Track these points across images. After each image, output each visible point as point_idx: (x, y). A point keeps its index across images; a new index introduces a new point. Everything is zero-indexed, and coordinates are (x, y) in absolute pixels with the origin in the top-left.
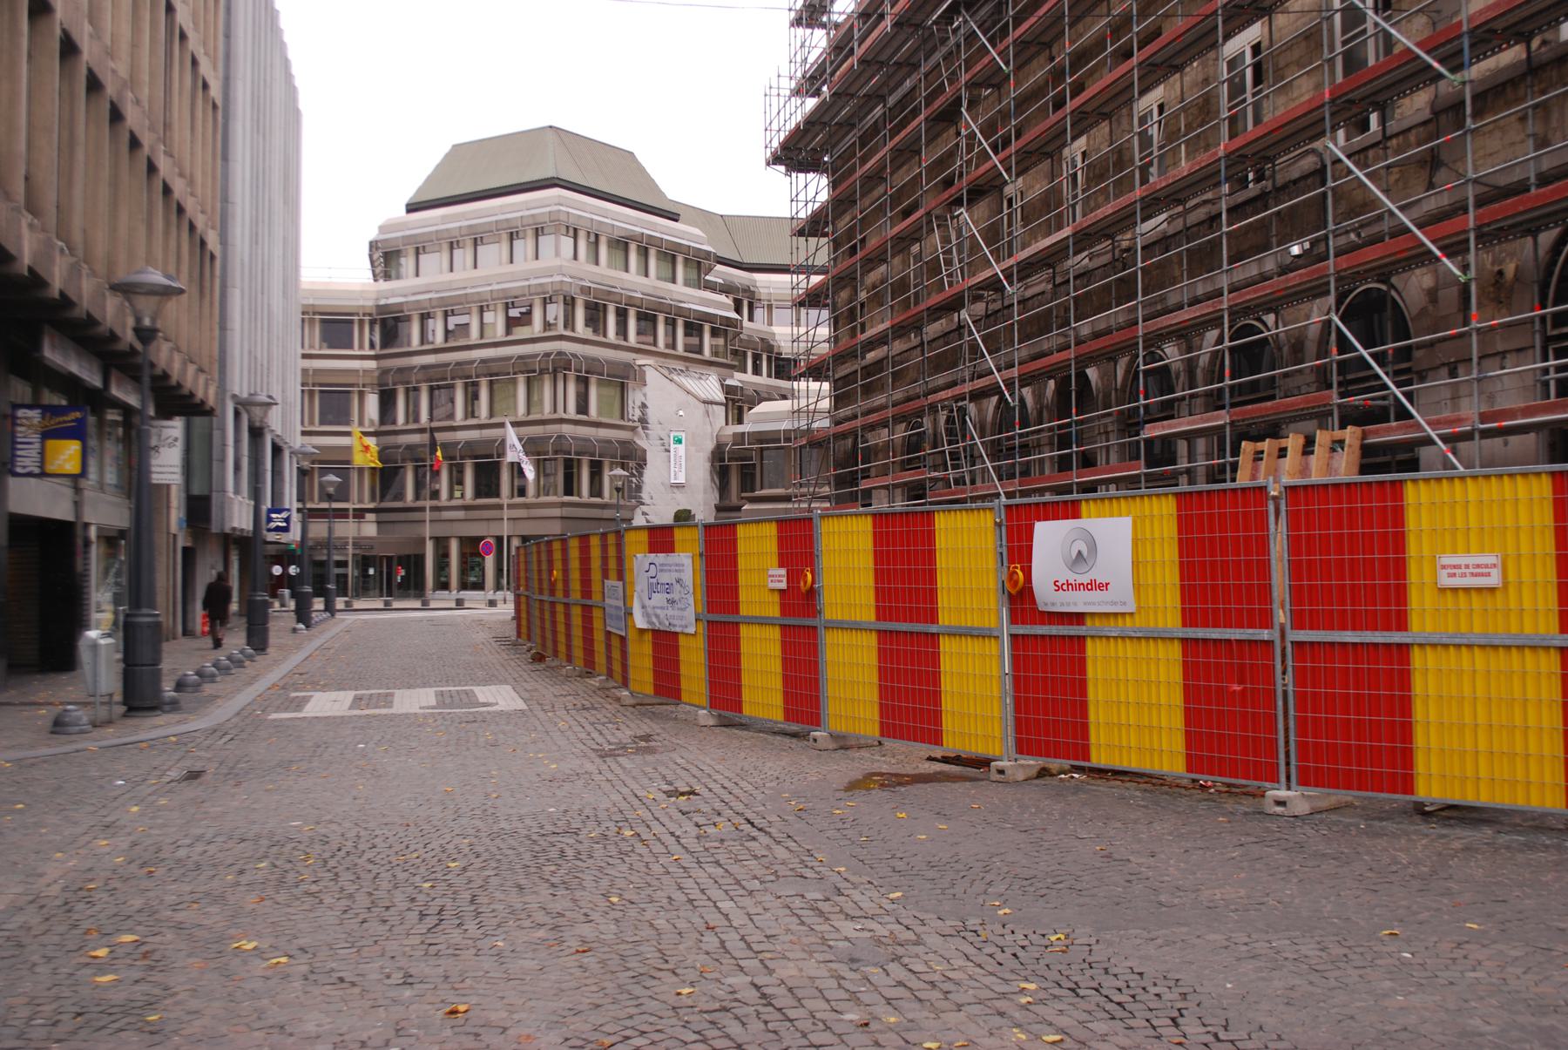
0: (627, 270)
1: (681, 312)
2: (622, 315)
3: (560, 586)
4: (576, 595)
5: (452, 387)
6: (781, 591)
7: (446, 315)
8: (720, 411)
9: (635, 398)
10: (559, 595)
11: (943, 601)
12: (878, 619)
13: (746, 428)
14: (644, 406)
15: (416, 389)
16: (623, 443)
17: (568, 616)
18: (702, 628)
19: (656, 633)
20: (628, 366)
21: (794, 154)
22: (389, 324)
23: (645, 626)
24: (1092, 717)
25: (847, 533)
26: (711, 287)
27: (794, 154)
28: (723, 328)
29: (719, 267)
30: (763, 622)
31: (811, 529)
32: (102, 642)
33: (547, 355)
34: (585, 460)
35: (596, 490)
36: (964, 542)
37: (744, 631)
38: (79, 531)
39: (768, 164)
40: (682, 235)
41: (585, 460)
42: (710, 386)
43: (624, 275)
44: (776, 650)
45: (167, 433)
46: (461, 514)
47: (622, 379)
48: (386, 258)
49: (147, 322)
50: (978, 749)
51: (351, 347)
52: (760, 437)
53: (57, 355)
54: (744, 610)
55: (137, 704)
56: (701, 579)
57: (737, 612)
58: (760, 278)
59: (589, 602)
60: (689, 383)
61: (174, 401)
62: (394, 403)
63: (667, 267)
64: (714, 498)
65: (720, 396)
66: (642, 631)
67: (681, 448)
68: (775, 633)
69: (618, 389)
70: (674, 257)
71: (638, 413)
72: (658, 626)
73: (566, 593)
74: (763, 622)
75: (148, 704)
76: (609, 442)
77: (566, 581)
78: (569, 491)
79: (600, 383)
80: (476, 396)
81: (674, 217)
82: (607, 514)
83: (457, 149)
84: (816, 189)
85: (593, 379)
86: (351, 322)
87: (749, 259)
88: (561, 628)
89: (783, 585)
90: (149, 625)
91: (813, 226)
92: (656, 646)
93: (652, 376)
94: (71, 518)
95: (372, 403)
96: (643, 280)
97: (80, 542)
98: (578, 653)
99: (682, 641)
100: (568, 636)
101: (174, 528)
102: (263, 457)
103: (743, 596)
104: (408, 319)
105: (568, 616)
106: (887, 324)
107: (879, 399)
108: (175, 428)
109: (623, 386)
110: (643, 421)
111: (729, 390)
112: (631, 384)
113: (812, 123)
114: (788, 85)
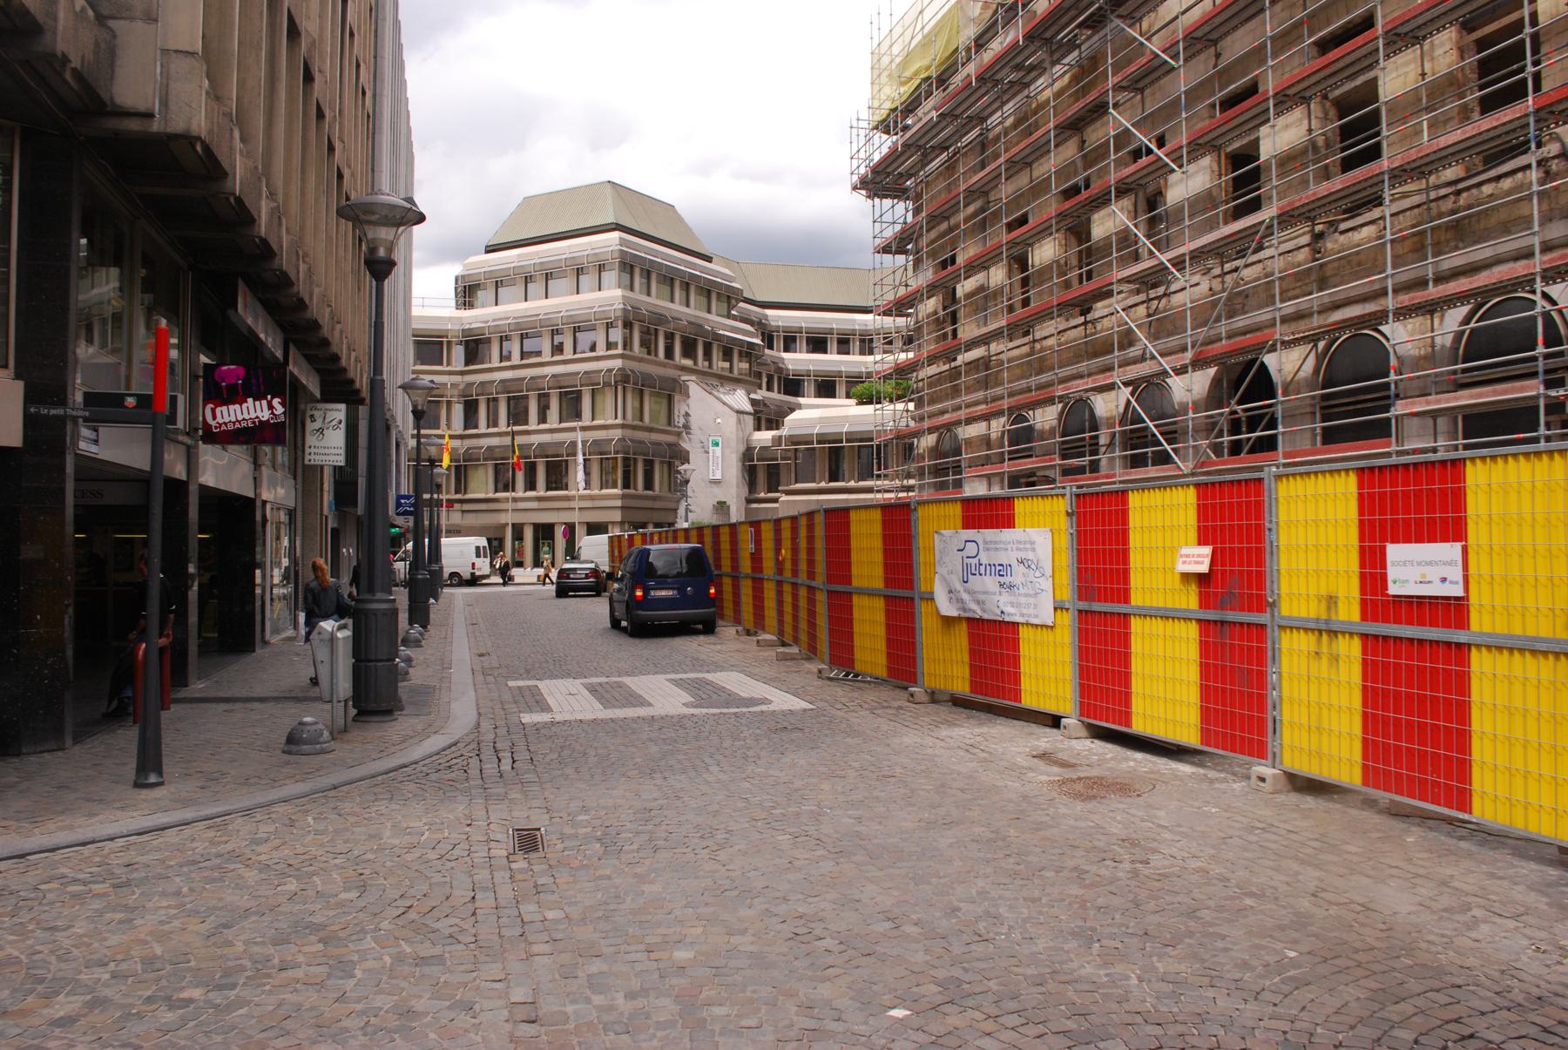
0: (672, 301)
1: (718, 337)
2: (670, 337)
3: (788, 565)
4: (802, 578)
5: (526, 397)
6: (1201, 579)
7: (522, 337)
8: (750, 420)
9: (680, 408)
10: (788, 574)
11: (1135, 580)
12: (1364, 617)
13: (784, 432)
14: (687, 414)
15: (496, 400)
16: (670, 445)
17: (795, 596)
18: (1067, 621)
19: (975, 623)
20: (675, 381)
21: (879, 182)
22: (475, 347)
23: (954, 613)
24: (1475, 725)
25: (1171, 506)
26: (735, 318)
27: (879, 182)
28: (748, 352)
29: (741, 304)
30: (871, 593)
31: (1259, 493)
32: (339, 635)
33: (610, 371)
34: (640, 459)
35: (649, 484)
36: (1314, 519)
37: (1136, 625)
38: (259, 503)
39: (855, 188)
40: (717, 274)
41: (640, 459)
42: (740, 399)
43: (671, 305)
44: (880, 616)
45: (331, 415)
46: (534, 505)
47: (670, 392)
48: (467, 292)
49: (382, 253)
50: (1050, 707)
51: (441, 364)
52: (794, 440)
53: (250, 316)
54: (1137, 599)
55: (372, 706)
56: (1067, 559)
57: (850, 583)
58: (769, 312)
59: (813, 584)
60: (727, 398)
61: (338, 387)
62: (476, 411)
63: (704, 300)
64: (745, 491)
65: (748, 408)
66: (948, 621)
67: (718, 450)
68: (1192, 630)
69: (665, 402)
70: (709, 292)
71: (682, 420)
72: (978, 612)
73: (795, 572)
74: (871, 593)
75: (384, 706)
76: (659, 444)
77: (795, 562)
78: (626, 485)
79: (652, 394)
80: (547, 407)
81: (709, 259)
82: (658, 505)
83: (528, 201)
84: (898, 212)
85: (647, 391)
86: (441, 343)
87: (759, 298)
88: (803, 614)
89: (1204, 568)
90: (385, 613)
91: (897, 245)
92: (973, 639)
93: (695, 389)
94: (251, 495)
95: (458, 411)
96: (684, 309)
97: (258, 517)
98: (803, 637)
99: (1024, 633)
100: (795, 618)
101: (326, 511)
102: (390, 449)
103: (854, 571)
104: (488, 341)
105: (795, 596)
106: (1003, 323)
107: (998, 391)
108: (339, 412)
109: (670, 399)
110: (687, 427)
111: (754, 402)
112: (677, 397)
113: (893, 157)
114: (867, 117)
